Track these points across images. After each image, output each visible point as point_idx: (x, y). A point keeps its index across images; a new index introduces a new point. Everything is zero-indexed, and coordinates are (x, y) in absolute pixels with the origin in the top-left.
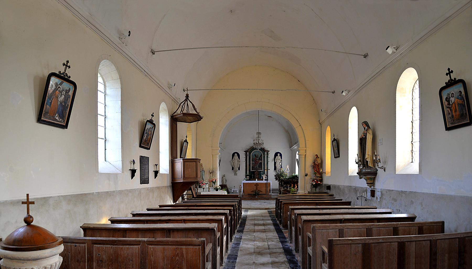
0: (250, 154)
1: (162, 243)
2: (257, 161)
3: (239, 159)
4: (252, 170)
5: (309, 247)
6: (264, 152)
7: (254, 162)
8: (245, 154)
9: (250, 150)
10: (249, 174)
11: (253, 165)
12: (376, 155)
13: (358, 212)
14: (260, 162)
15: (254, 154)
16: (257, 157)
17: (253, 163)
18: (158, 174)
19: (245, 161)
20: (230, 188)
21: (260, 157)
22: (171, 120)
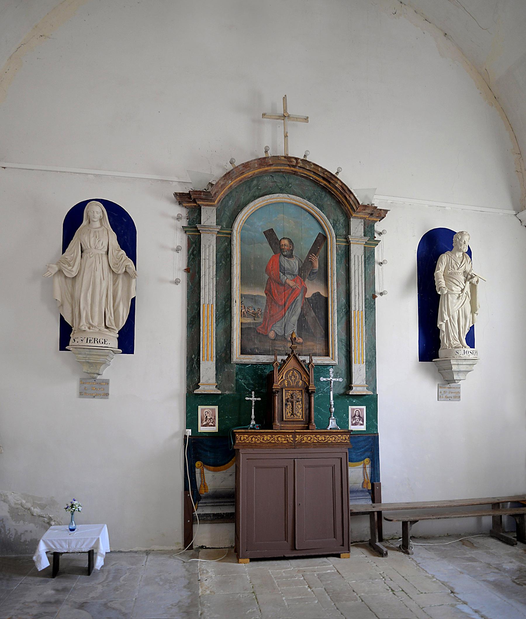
0: (231, 226)
1: (287, 151)
2: (284, 285)
3: (132, 255)
4: (243, 352)
5: (368, 543)
6: (342, 219)
7: (262, 293)
8: (185, 223)
9: (229, 195)
10: (212, 389)
11: (255, 315)
12: (74, 333)
13: (358, 394)
14: (309, 295)
15: (261, 226)
16: (291, 256)
17: (254, 299)
18: (436, 284)
19: (183, 277)
20: (37, 511)
21: (314, 250)
22: (378, 467)
